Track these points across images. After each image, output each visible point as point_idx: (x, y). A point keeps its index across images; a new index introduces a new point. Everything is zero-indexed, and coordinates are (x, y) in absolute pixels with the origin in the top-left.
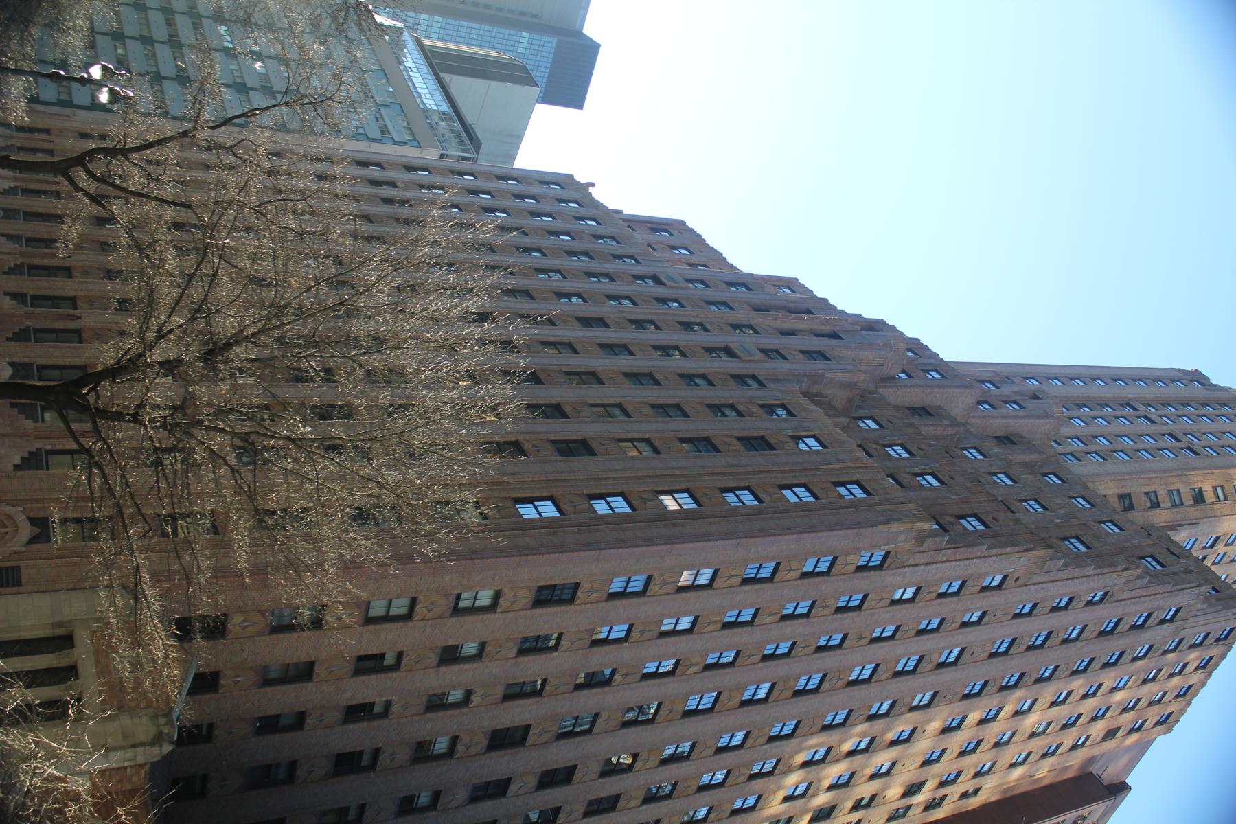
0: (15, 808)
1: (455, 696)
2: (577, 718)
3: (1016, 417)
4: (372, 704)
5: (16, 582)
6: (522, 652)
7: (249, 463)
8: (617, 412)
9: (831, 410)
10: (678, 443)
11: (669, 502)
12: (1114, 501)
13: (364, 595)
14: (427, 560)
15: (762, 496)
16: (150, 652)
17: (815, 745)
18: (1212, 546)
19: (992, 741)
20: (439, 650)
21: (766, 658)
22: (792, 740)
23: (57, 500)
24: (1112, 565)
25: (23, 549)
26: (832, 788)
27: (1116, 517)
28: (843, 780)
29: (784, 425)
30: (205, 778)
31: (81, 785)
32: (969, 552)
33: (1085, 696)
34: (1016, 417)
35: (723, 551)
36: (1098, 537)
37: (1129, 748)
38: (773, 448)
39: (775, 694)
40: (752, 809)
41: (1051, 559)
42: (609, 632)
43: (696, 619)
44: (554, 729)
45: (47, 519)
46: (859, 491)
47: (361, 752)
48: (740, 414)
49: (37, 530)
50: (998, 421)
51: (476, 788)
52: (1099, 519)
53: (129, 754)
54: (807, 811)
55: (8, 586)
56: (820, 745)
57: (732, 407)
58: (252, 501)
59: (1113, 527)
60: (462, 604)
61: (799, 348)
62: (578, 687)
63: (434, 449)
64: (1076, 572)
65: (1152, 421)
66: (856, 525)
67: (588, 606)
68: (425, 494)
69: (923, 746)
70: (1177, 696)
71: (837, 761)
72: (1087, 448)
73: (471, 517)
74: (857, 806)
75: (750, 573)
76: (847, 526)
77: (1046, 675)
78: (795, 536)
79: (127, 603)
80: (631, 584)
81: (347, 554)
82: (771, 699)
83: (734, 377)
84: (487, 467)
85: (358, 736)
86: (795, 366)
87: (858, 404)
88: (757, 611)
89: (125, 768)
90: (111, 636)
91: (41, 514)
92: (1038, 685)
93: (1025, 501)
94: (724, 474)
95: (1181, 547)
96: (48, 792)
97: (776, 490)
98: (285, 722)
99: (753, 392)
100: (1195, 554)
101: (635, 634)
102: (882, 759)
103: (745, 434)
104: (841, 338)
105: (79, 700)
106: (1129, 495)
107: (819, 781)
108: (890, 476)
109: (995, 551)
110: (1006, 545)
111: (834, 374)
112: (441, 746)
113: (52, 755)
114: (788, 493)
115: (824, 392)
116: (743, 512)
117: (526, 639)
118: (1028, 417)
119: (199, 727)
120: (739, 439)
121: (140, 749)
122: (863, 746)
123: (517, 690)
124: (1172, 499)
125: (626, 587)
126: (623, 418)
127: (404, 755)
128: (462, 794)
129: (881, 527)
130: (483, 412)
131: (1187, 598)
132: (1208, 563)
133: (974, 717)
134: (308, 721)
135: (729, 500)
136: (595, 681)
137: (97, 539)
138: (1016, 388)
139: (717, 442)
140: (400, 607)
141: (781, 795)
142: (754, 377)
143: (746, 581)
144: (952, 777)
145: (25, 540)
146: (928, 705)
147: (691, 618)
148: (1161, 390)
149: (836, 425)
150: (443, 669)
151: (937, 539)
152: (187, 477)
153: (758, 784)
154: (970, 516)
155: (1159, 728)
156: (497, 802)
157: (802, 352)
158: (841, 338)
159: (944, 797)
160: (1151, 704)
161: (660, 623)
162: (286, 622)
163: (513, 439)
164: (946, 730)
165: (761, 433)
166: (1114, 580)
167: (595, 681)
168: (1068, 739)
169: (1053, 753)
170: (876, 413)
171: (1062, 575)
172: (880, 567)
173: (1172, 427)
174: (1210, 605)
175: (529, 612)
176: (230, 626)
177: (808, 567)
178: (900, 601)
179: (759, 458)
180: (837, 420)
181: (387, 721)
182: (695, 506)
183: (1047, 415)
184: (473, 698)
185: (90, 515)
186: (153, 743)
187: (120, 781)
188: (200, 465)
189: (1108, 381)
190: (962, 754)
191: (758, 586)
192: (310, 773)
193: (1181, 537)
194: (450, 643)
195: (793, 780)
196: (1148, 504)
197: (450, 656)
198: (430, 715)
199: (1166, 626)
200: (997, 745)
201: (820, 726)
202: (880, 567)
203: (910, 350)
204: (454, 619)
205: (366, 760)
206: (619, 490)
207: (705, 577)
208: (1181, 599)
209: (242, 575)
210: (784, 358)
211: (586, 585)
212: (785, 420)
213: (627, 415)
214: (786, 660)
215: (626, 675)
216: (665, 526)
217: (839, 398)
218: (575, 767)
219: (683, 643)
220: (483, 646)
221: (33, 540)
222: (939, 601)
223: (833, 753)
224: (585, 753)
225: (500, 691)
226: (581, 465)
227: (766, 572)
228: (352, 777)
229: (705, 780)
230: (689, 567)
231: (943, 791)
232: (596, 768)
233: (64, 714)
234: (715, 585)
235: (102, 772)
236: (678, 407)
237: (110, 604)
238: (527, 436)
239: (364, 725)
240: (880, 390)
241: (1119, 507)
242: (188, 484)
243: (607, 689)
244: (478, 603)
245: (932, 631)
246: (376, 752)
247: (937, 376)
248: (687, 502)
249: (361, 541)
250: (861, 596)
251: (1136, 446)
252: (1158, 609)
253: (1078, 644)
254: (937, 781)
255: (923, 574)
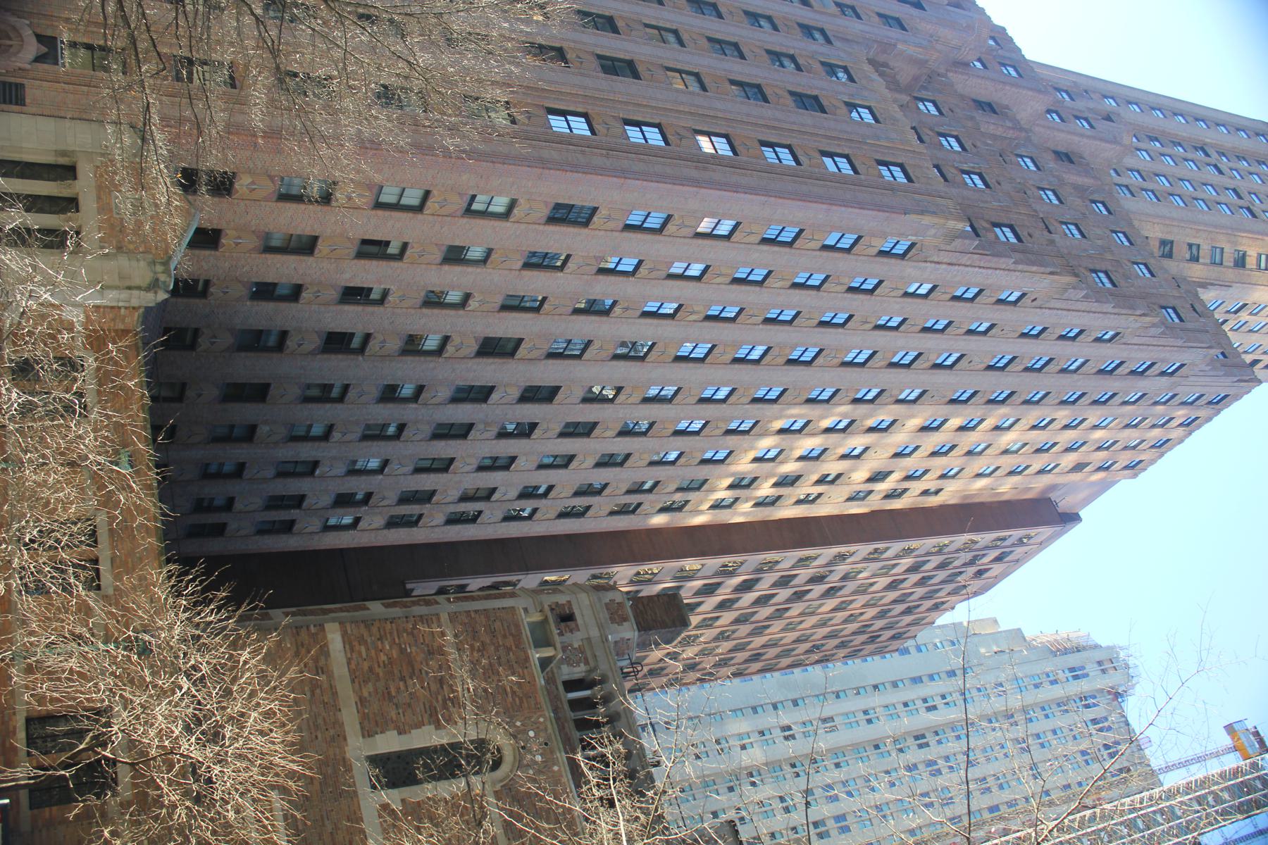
0: (11, 326)
1: (454, 297)
2: (569, 342)
3: (1082, 136)
4: (370, 289)
5: (20, 101)
6: (527, 266)
7: (276, 18)
8: (671, 38)
9: (894, 85)
10: (727, 84)
11: (705, 144)
12: (1155, 246)
13: (378, 178)
14: (447, 154)
15: (801, 158)
16: (153, 196)
17: (795, 414)
18: (1236, 312)
19: (966, 449)
20: (444, 248)
21: (768, 321)
22: (775, 406)
23: (67, 20)
24: (1132, 308)
25: (28, 67)
26: (801, 458)
27: (1151, 262)
28: (815, 454)
29: (841, 88)
30: (196, 332)
31: (76, 317)
32: (994, 262)
33: (1066, 427)
34: (1082, 136)
35: (749, 206)
36: (1126, 277)
37: (1093, 483)
38: (824, 111)
39: (768, 358)
40: (722, 461)
41: (1074, 288)
42: (618, 263)
43: (707, 267)
44: (546, 348)
45: (55, 38)
46: (901, 175)
47: (353, 334)
48: (798, 68)
49: (44, 50)
50: (1062, 135)
51: (460, 390)
52: (1134, 259)
53: (125, 295)
54: (773, 475)
55: (11, 103)
56: (800, 416)
57: (792, 58)
58: (275, 58)
59: (1145, 271)
60: (475, 207)
61: (877, 10)
62: (577, 311)
63: (472, 38)
64: (1095, 306)
65: (1220, 172)
66: (890, 209)
67: (602, 233)
68: (455, 83)
69: (898, 439)
70: (1153, 447)
71: (813, 435)
72: (1145, 185)
73: (500, 118)
74: (821, 481)
75: (771, 234)
76: (880, 208)
77: (1035, 399)
78: (824, 206)
79: (133, 145)
80: (649, 220)
81: (367, 132)
82: (763, 362)
83: (801, 26)
84: (529, 69)
85: (351, 319)
86: (867, 28)
87: (923, 85)
88: (770, 273)
89: (119, 308)
90: (116, 173)
91: (49, 33)
92: (1025, 406)
93: (1066, 224)
94: (768, 127)
95: (1205, 306)
96: (43, 317)
97: (817, 155)
98: (279, 291)
99: (817, 47)
100: (1216, 316)
101: (643, 271)
102: (857, 442)
103: (799, 90)
104: (923, 9)
105: (78, 233)
106: (1172, 242)
107: (792, 449)
108: (937, 167)
109: (1020, 267)
110: (1033, 263)
111: (907, 47)
112: (431, 343)
113: (49, 282)
114: (828, 161)
115: (891, 64)
116: (776, 171)
117: (534, 254)
118: (1094, 138)
119: (196, 281)
120: (792, 93)
121: (135, 292)
122: (841, 426)
123: (516, 303)
124: (1213, 256)
125: (644, 222)
126: (677, 46)
127: (395, 344)
128: (445, 393)
129: (913, 217)
130: (531, 8)
131: (1194, 357)
132: (1226, 328)
133: (955, 422)
134: (304, 294)
135: (767, 154)
136: (592, 309)
137: (106, 69)
138: (1091, 105)
139: (768, 91)
140: (412, 198)
141: (752, 455)
142: (822, 31)
143: (765, 241)
144: (918, 474)
145: (31, 57)
146: (914, 401)
147: (702, 267)
148: (1242, 141)
149: (895, 101)
150: (446, 268)
151: (967, 242)
152: (209, 19)
153: (732, 440)
154: (1006, 226)
155: (1126, 472)
156: (477, 406)
157: (880, 15)
158: (923, 9)
159: (905, 490)
160: (1126, 448)
161: (670, 264)
162: (294, 191)
163: (557, 45)
164: (924, 429)
165: (815, 93)
166: (1129, 323)
167: (592, 309)
168: (1038, 463)
169: (1020, 473)
170: (939, 100)
171: (1079, 306)
172: (903, 256)
173: (1238, 182)
174: (1214, 369)
175: (541, 227)
176: (237, 186)
177: (831, 241)
178: (913, 295)
179: (808, 119)
180: (897, 96)
181: (381, 309)
182: (731, 154)
183: (1114, 141)
184: (470, 302)
185: (101, 42)
186: (148, 289)
187: (113, 320)
188: (223, 10)
189: (1190, 119)
190: (934, 454)
191: (776, 249)
192: (300, 345)
193: (1209, 296)
194: (457, 243)
195: (766, 444)
196: (1188, 256)
197: (455, 256)
198: (425, 311)
199: (1165, 379)
200: (970, 453)
201: (805, 398)
202: (903, 256)
203: (993, 38)
204: (465, 220)
205: (356, 343)
206: (657, 121)
207: (724, 229)
208: (1185, 357)
209: (255, 136)
210: (859, 17)
211: (603, 212)
212: (844, 84)
213: (681, 43)
214: (787, 328)
215: (627, 309)
216: (696, 168)
217: (905, 73)
218: (559, 388)
219: (689, 289)
220: (489, 252)
221: (39, 59)
222: (952, 303)
223: (810, 426)
224: (573, 377)
225: (499, 300)
226: (623, 85)
227: (787, 237)
228: (340, 356)
229: (682, 425)
230: (712, 215)
231: (906, 485)
232: (579, 393)
233: (61, 245)
234: (734, 238)
235: (97, 307)
236: (736, 46)
237: (119, 143)
238: (572, 45)
239: (360, 308)
240: (950, 74)
241: (1157, 252)
242: (209, 27)
243: (604, 319)
244: (491, 209)
245: (937, 331)
246: (367, 337)
247: (1013, 73)
248: (723, 148)
249: (383, 121)
250: (876, 281)
251: (1196, 194)
252: (1163, 361)
253: (1075, 376)
254: (903, 474)
255: (942, 273)
